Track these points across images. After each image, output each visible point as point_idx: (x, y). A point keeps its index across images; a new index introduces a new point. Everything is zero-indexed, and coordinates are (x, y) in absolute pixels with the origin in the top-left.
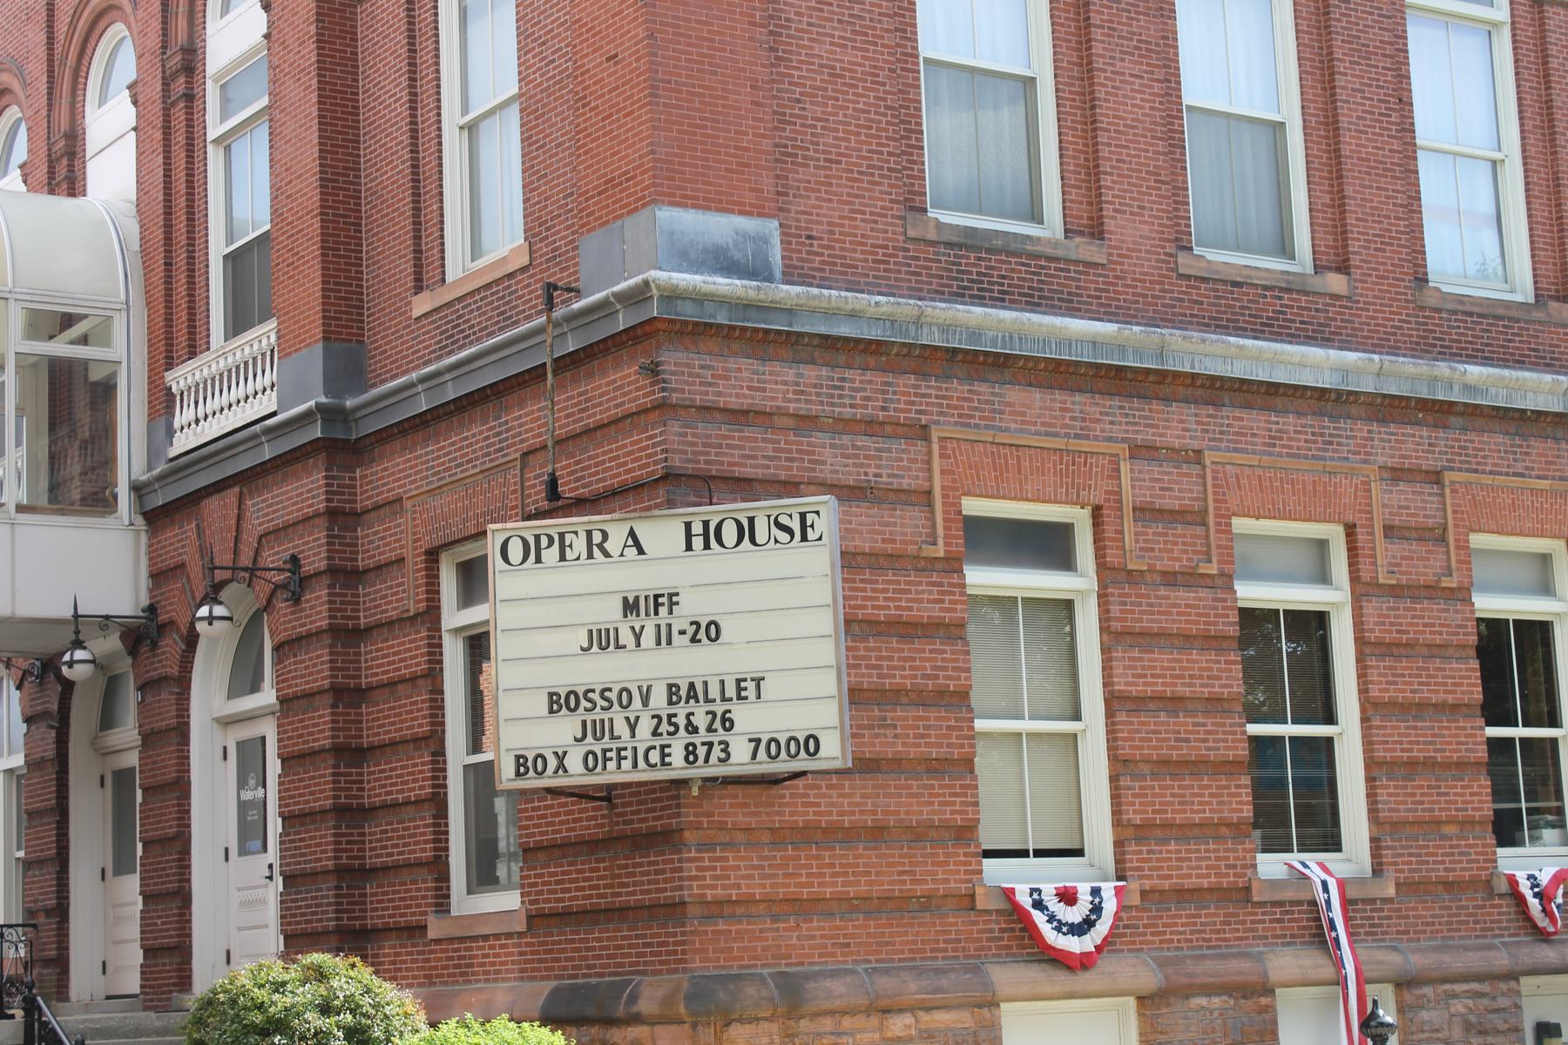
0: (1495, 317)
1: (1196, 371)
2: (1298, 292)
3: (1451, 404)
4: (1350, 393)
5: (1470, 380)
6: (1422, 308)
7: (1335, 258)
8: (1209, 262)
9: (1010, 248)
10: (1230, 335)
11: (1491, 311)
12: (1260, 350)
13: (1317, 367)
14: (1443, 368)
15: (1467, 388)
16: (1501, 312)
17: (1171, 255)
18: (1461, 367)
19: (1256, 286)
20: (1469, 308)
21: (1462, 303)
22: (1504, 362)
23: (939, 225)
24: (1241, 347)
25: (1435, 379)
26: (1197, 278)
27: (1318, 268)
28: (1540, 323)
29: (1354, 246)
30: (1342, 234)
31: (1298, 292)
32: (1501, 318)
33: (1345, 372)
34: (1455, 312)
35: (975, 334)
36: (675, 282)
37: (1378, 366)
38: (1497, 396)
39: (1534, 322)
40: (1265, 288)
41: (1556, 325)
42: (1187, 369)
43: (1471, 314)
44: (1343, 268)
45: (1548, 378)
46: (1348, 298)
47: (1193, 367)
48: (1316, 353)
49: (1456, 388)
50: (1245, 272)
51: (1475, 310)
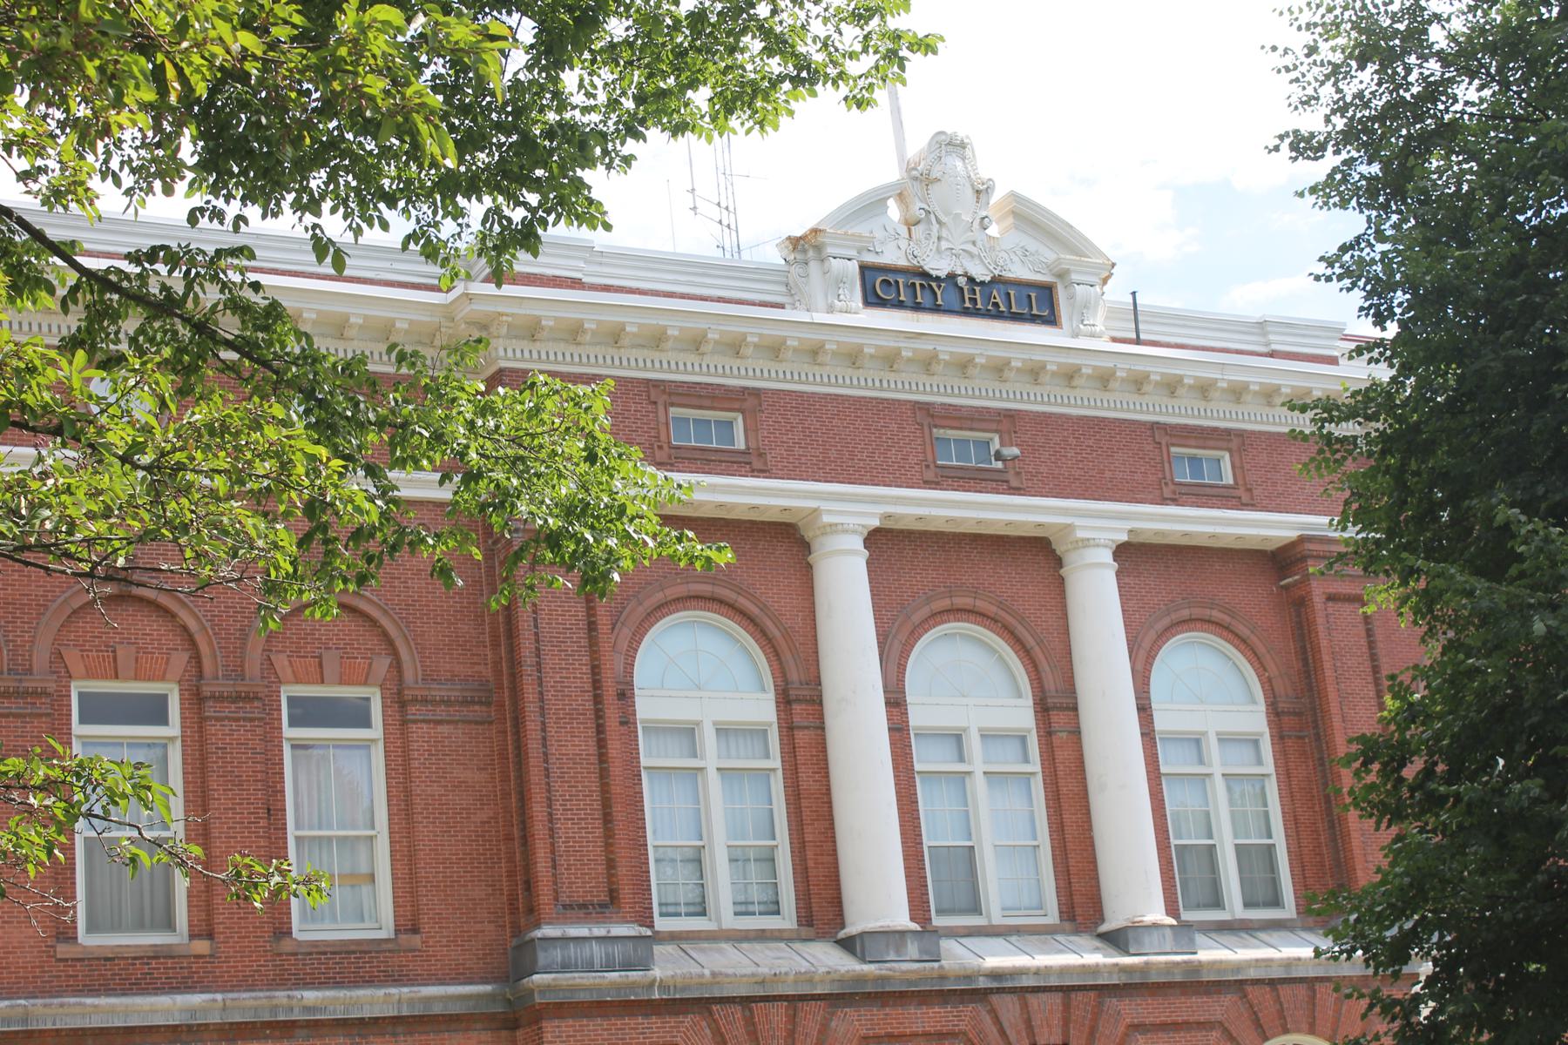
0: (347, 952)
1: (58, 1026)
2: (165, 957)
3: (295, 1021)
4: (199, 1025)
5: (305, 1002)
6: (280, 955)
7: (203, 929)
8: (85, 947)
9: (158, 955)
10: (276, 990)
11: (344, 949)
12: (113, 1006)
13: (168, 1011)
14: (281, 995)
15: (307, 1009)
16: (353, 948)
17: (52, 947)
18: (297, 994)
19: (127, 958)
20: (323, 949)
21: (316, 946)
22: (338, 985)
23: (300, 943)
24: (95, 1006)
25: (276, 1006)
26: (72, 960)
27: (192, 936)
28: (390, 951)
29: (219, 919)
30: (209, 910)
31: (165, 957)
32: (354, 952)
33: (193, 1011)
34: (311, 954)
35: (573, 989)
36: (631, 979)
37: (221, 1004)
38: (335, 1011)
39: (385, 951)
40: (135, 958)
41: (404, 951)
42: (49, 1026)
43: (325, 953)
44: (210, 936)
45: (381, 992)
46: (211, 956)
47: (54, 1024)
48: (164, 1001)
49: (296, 1010)
50: (117, 950)
51: (329, 949)
